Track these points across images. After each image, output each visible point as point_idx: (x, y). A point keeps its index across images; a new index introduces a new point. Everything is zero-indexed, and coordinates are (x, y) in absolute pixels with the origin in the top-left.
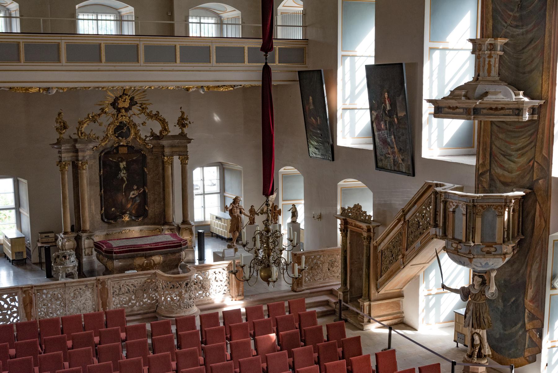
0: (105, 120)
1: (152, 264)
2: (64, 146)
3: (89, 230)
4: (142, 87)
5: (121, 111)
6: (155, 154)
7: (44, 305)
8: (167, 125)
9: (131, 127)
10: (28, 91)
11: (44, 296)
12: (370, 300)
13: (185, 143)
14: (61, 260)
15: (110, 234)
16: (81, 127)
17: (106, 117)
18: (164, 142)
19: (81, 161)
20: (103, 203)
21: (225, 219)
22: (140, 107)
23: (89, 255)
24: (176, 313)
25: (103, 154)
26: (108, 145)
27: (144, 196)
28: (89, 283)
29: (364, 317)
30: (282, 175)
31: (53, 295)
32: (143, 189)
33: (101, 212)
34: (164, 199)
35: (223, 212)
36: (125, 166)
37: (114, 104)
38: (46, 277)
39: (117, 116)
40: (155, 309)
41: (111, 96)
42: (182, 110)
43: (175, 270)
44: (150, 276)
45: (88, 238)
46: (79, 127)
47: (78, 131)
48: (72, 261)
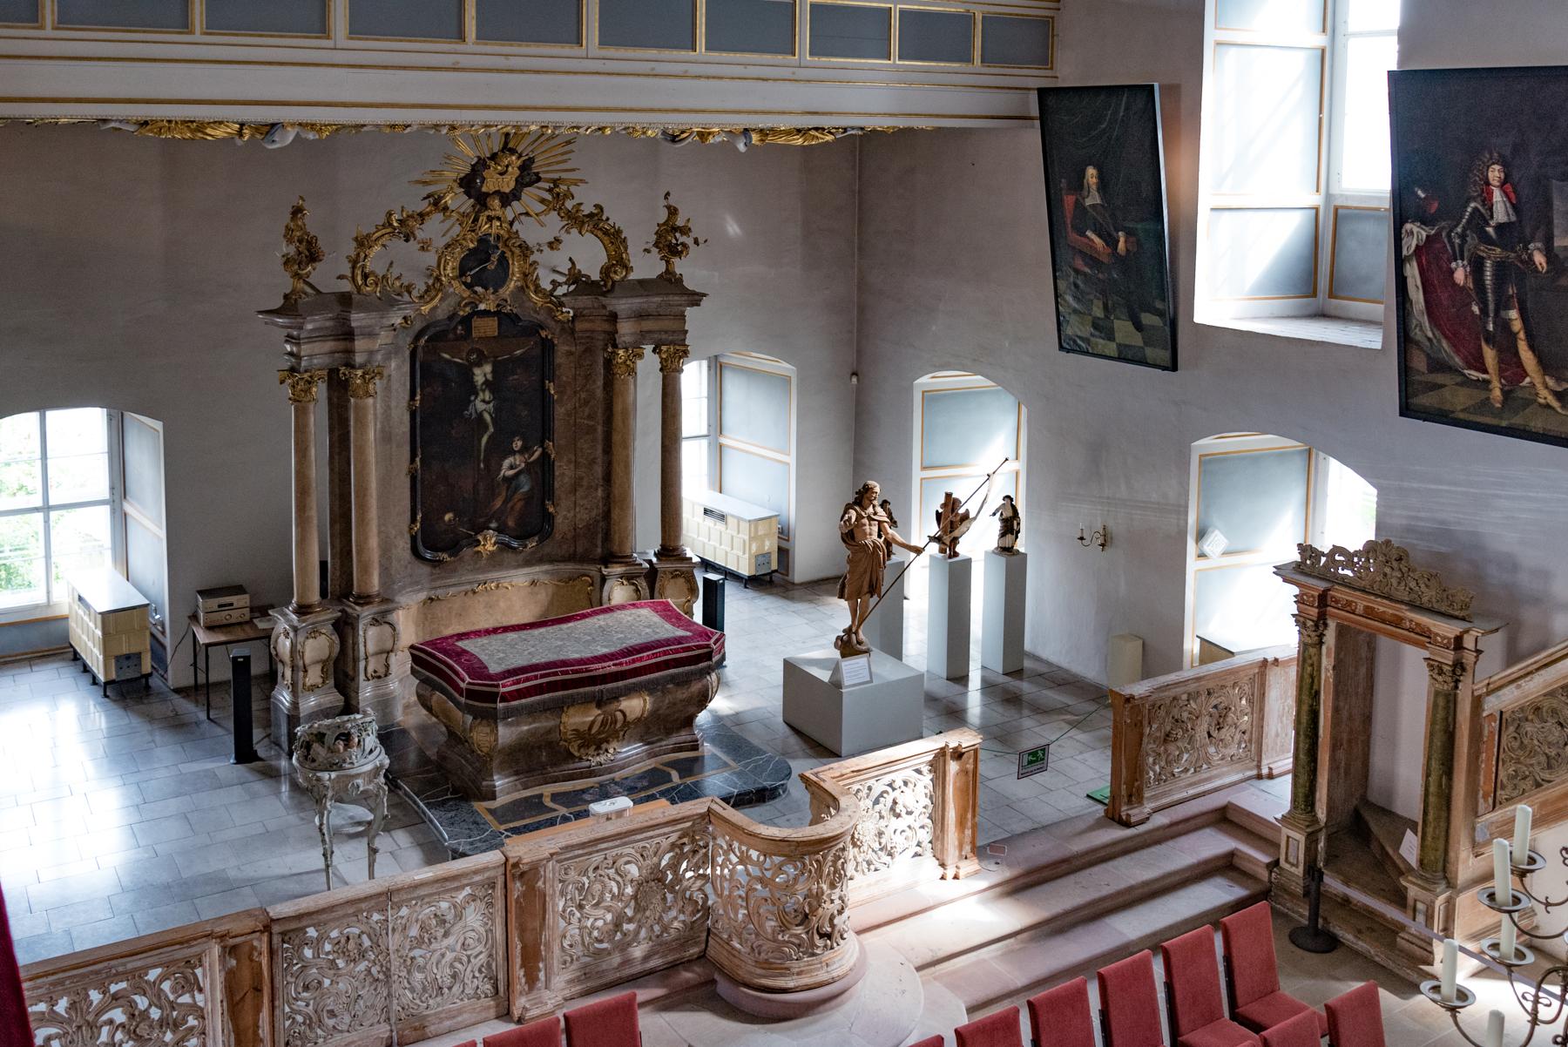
0: (436, 230)
3: (378, 595)
4: (578, 128)
6: (582, 338)
7: (306, 988)
9: (513, 253)
10: (200, 135)
11: (308, 953)
12: (1450, 885)
13: (680, 305)
14: (331, 750)
15: (438, 599)
16: (362, 255)
17: (443, 222)
18: (622, 305)
21: (739, 519)
22: (550, 190)
23: (379, 677)
24: (799, 974)
25: (422, 341)
26: (439, 310)
27: (543, 470)
29: (1431, 944)
30: (923, 392)
31: (343, 941)
32: (540, 449)
34: (608, 478)
35: (714, 490)
36: (489, 377)
37: (469, 183)
38: (232, 761)
40: (703, 946)
41: (468, 153)
42: (672, 201)
43: (683, 733)
44: (689, 824)
45: (376, 622)
46: (358, 255)
47: (354, 268)
48: (368, 750)
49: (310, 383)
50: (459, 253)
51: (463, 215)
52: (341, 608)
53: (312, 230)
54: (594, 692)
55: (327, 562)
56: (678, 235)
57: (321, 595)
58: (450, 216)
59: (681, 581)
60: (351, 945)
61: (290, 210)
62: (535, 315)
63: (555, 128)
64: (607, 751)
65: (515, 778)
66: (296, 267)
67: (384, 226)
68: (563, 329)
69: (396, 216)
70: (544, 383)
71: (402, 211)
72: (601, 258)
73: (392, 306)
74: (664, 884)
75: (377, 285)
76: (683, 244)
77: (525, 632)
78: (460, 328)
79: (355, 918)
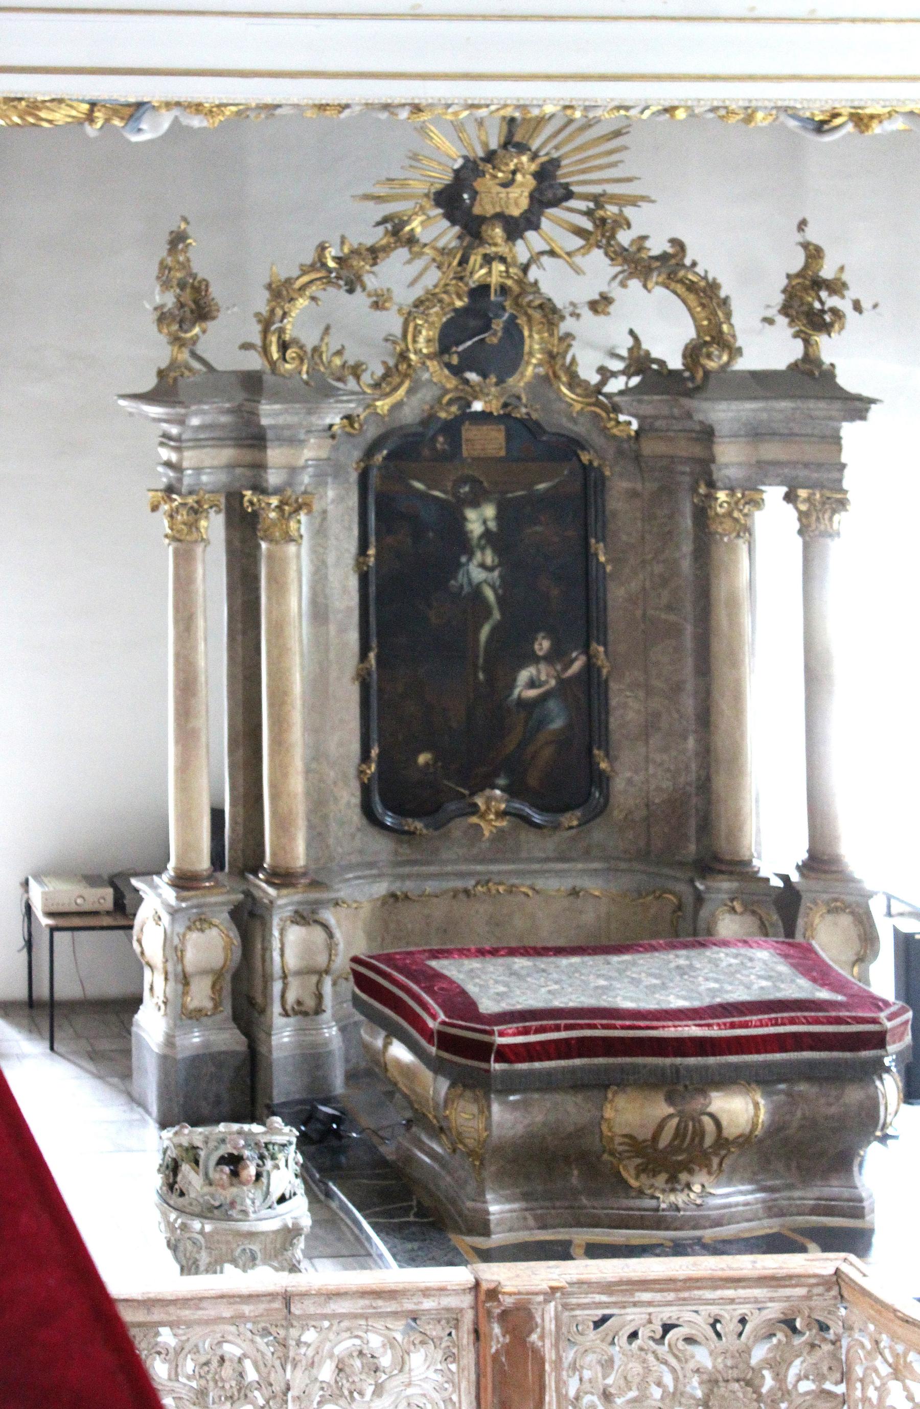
1: (709, 1141)
2: (196, 413)
3: (304, 874)
5: (487, 231)
8: (728, 315)
9: (530, 319)
10: (31, 120)
13: (831, 418)
16: (279, 312)
17: (409, 262)
19: (277, 491)
20: (374, 726)
22: (589, 213)
25: (379, 458)
28: (428, 1304)
31: (215, 1363)
33: (361, 772)
36: (492, 525)
39: (464, 261)
42: (812, 235)
43: (834, 1182)
44: (801, 1291)
45: (302, 918)
46: (272, 311)
47: (265, 332)
49: (196, 512)
50: (438, 316)
51: (442, 251)
52: (245, 887)
53: (201, 267)
54: (663, 1069)
55: (222, 812)
56: (824, 294)
57: (213, 862)
58: (421, 254)
59: (845, 920)
60: (227, 1371)
61: (167, 237)
62: (570, 425)
63: (587, 109)
64: (688, 1186)
65: (523, 1205)
66: (175, 327)
67: (312, 267)
68: (620, 452)
69: (331, 252)
70: (587, 545)
71: (342, 243)
72: (686, 331)
73: (327, 396)
74: (757, 1391)
75: (302, 360)
76: (835, 311)
77: (545, 959)
78: (441, 439)
79: (233, 1329)
